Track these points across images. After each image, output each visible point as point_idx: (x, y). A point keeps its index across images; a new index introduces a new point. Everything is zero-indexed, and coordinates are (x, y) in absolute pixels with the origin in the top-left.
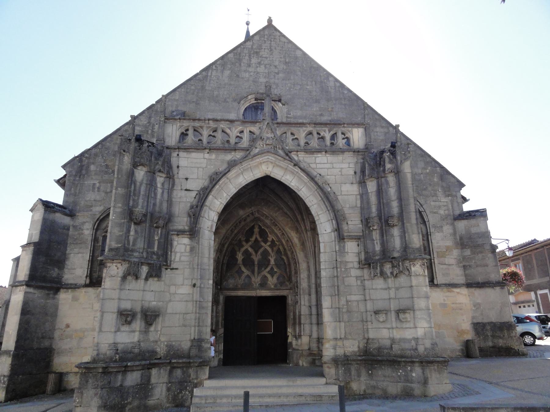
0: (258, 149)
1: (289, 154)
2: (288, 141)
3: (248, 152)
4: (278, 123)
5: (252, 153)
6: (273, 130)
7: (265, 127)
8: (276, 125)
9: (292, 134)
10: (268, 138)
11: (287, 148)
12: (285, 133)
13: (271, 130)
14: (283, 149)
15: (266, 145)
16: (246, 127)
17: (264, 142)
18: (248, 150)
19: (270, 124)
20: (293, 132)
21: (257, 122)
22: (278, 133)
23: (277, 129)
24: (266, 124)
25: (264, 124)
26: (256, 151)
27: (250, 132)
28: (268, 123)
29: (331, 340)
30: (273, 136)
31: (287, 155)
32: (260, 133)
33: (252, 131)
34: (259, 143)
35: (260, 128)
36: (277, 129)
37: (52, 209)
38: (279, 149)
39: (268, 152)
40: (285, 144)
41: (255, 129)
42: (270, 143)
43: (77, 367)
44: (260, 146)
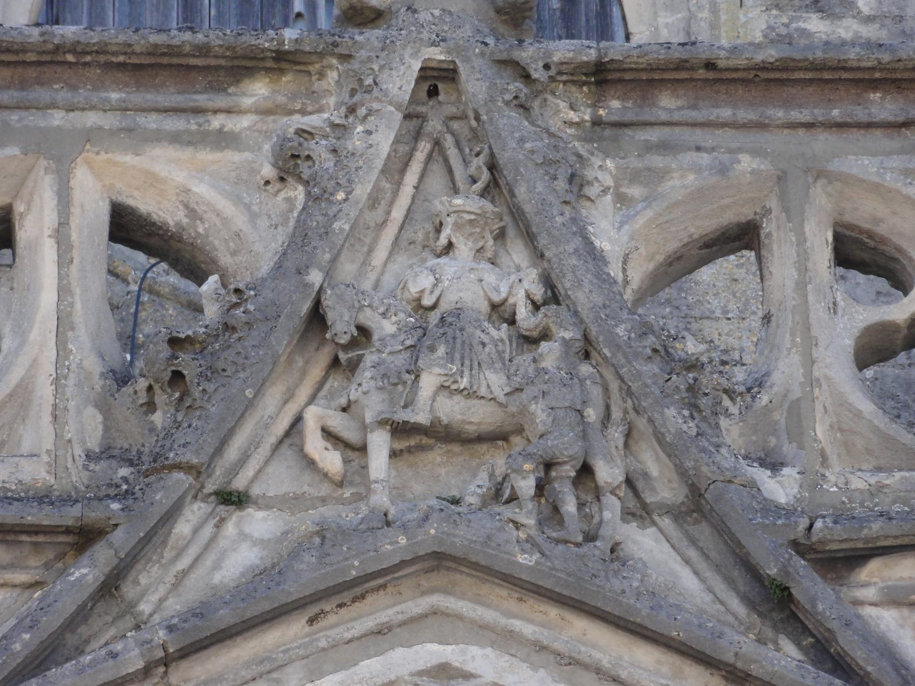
0: (259, 523)
1: (809, 586)
2: (786, 372)
3: (86, 573)
4: (601, 77)
5: (158, 595)
6: (531, 189)
7: (380, 137)
8: (566, 111)
9: (857, 252)
10: (433, 326)
11: (781, 488)
12: (743, 237)
13: (495, 184)
14: (699, 508)
15: (413, 437)
16: (61, 153)
17: (369, 394)
18: (85, 537)
19: (476, 83)
20: (866, 212)
21: (241, 66)
22: (622, 234)
23: (603, 171)
24: (401, 81)
25: (360, 89)
26: (242, 547)
27: (126, 227)
28: (436, 80)
29: (511, 101)
30: (518, 282)
31: (777, 604)
32: (302, 241)
33: (144, 203)
34: (272, 411)
35: (291, 163)
36: (603, 171)
37: (193, 492)
38: (640, 511)
39: (440, 561)
40: (732, 431)
41: (206, 176)
42: (477, 415)
43: (700, 248)
44: (289, 469)
